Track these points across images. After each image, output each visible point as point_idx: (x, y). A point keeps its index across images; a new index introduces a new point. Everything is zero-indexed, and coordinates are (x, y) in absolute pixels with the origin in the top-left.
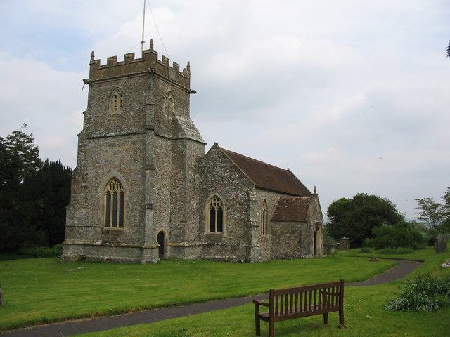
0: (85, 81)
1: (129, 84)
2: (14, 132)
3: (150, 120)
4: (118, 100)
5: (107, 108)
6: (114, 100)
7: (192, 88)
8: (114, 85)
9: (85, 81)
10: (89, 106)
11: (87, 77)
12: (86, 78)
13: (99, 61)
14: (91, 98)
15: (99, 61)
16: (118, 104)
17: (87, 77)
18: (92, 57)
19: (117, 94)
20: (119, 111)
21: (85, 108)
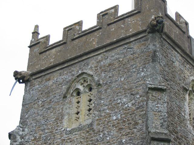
0: (19, 77)
1: (108, 61)
2: (178, 15)
3: (158, 123)
4: (84, 98)
5: (59, 119)
6: (74, 100)
7: (21, 87)
8: (76, 70)
9: (19, 77)
10: (23, 122)
11: (23, 68)
12: (19, 70)
13: (47, 38)
14: (27, 106)
15: (47, 38)
16: (84, 106)
17: (23, 68)
18: (35, 33)
19: (81, 88)
20: (85, 120)
21: (14, 123)
